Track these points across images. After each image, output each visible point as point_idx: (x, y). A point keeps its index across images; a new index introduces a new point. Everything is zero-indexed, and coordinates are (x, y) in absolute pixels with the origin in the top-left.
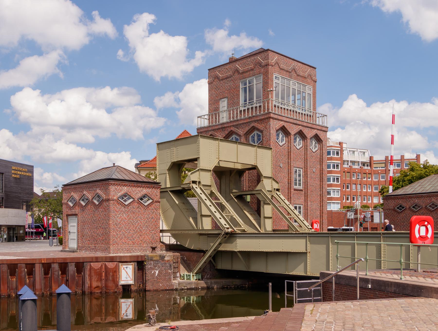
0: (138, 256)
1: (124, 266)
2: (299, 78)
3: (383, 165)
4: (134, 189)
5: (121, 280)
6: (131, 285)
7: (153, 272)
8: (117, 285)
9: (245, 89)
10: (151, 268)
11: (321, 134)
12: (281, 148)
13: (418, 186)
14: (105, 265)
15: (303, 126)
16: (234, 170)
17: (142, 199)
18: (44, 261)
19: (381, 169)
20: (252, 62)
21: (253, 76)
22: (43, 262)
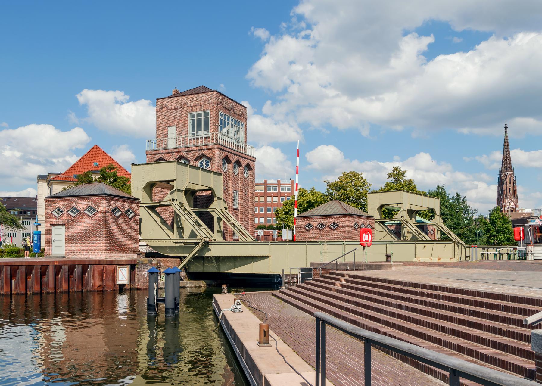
0: (132, 261)
1: (121, 268)
2: (235, 115)
3: (263, 188)
4: (122, 203)
5: (118, 281)
6: (125, 284)
7: (143, 274)
8: (115, 285)
9: (193, 121)
10: (142, 270)
11: (251, 163)
12: (225, 173)
13: (321, 209)
14: (106, 267)
15: (240, 156)
16: (190, 190)
17: (113, 211)
18: (57, 263)
19: (260, 191)
20: (200, 99)
21: (201, 111)
22: (56, 264)
